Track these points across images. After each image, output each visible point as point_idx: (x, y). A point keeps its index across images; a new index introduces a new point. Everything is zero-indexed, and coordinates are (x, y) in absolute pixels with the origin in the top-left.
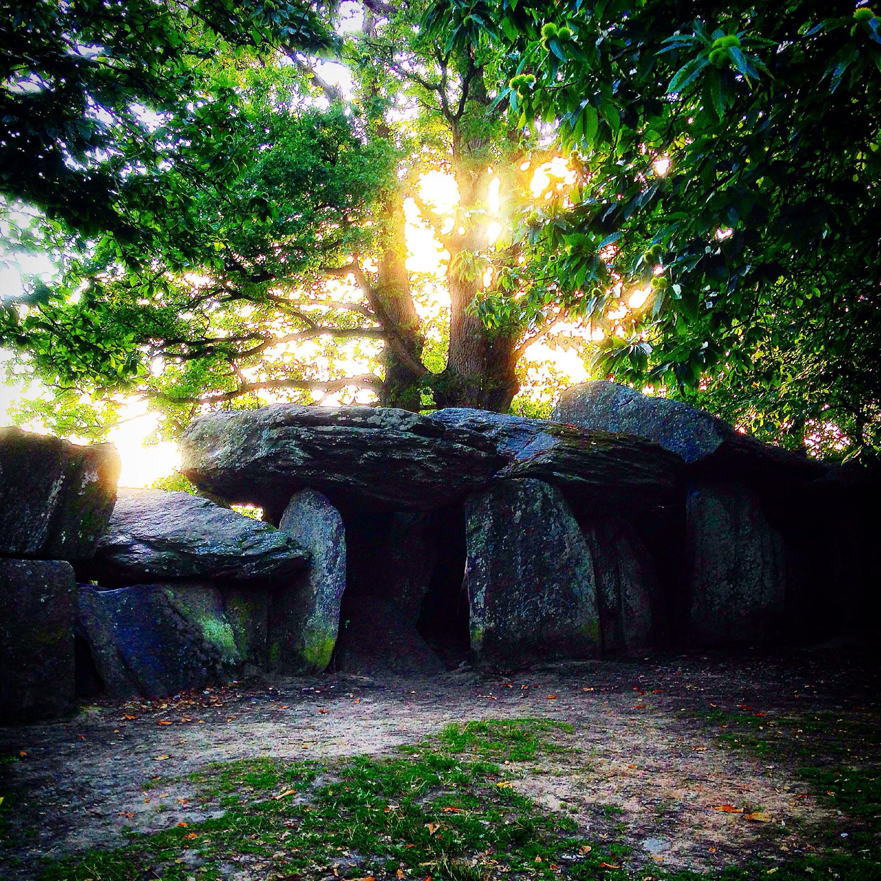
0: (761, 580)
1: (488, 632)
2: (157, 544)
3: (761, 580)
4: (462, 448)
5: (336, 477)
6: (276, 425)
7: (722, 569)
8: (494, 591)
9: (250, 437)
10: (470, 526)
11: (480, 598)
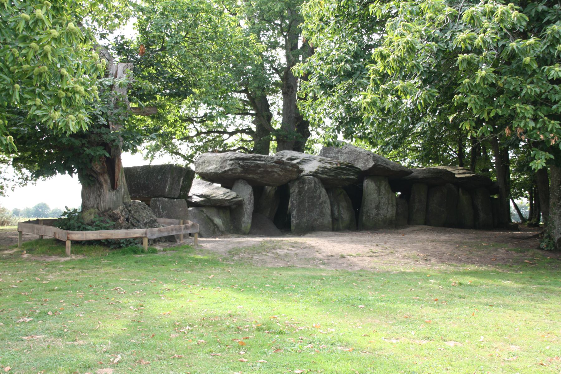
0: (387, 209)
1: (297, 223)
2: (201, 196)
3: (387, 209)
4: (276, 88)
5: (251, 176)
6: (231, 160)
7: (374, 205)
8: (299, 211)
9: (222, 163)
10: (291, 191)
11: (294, 213)
